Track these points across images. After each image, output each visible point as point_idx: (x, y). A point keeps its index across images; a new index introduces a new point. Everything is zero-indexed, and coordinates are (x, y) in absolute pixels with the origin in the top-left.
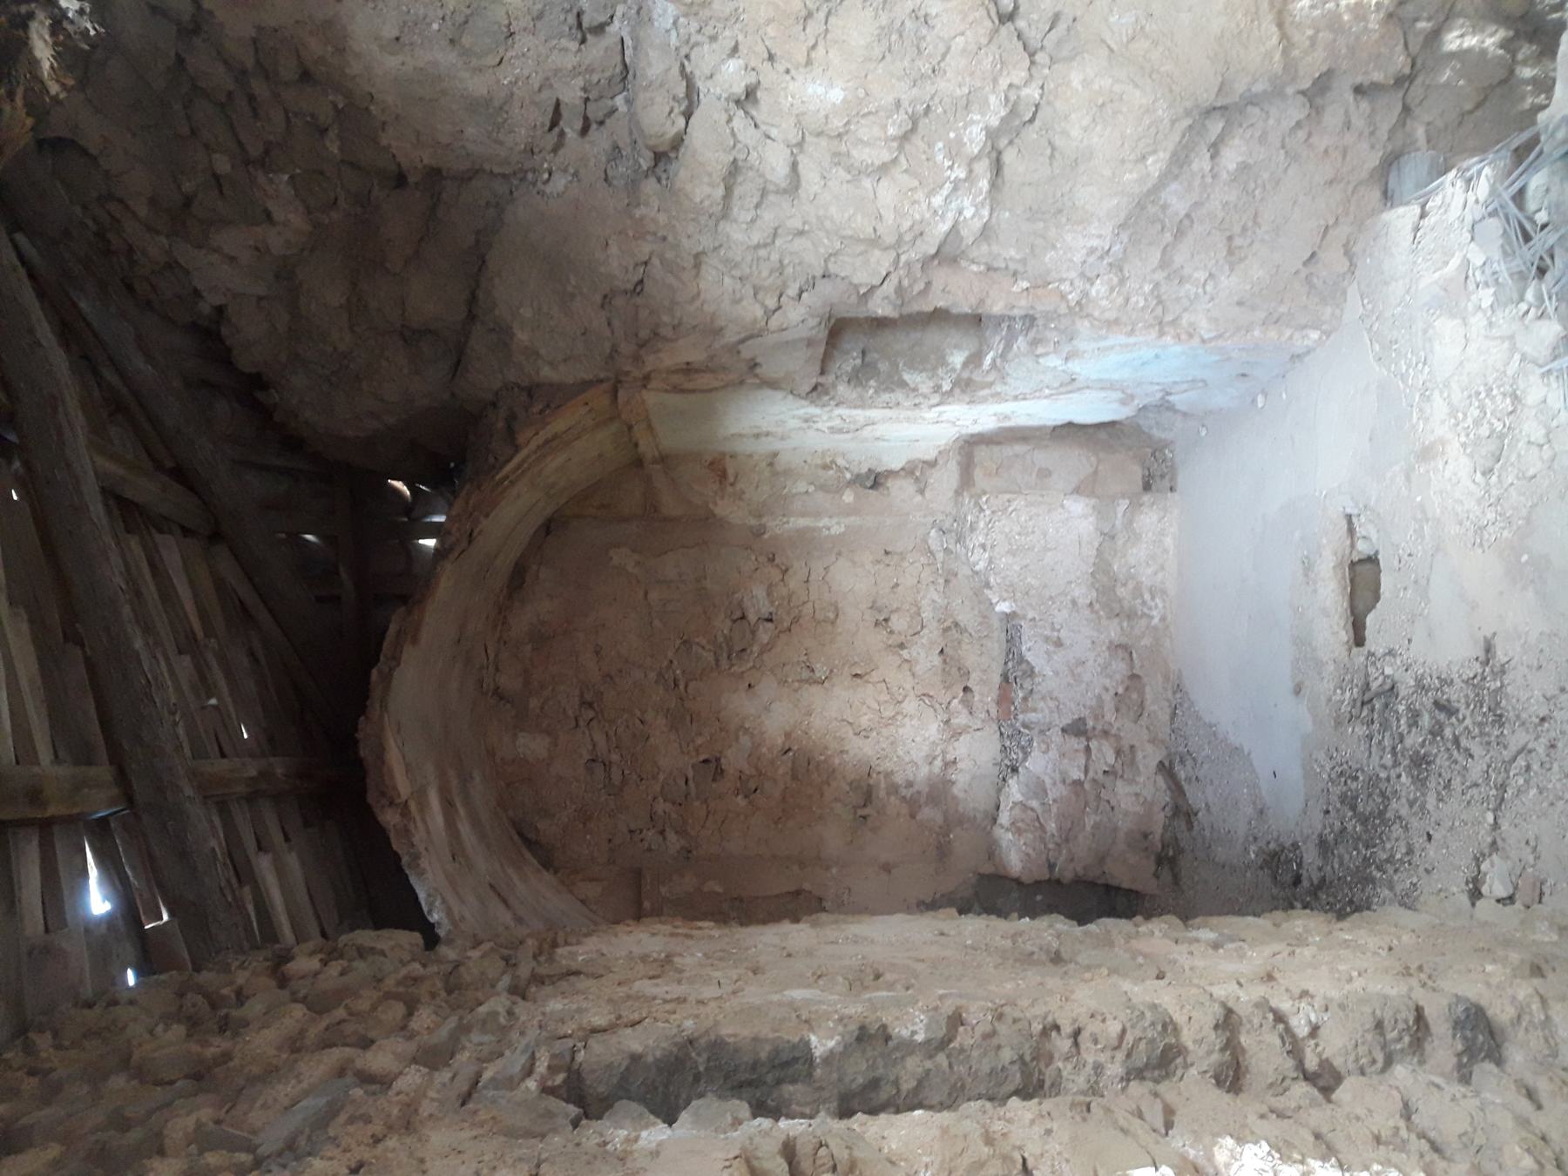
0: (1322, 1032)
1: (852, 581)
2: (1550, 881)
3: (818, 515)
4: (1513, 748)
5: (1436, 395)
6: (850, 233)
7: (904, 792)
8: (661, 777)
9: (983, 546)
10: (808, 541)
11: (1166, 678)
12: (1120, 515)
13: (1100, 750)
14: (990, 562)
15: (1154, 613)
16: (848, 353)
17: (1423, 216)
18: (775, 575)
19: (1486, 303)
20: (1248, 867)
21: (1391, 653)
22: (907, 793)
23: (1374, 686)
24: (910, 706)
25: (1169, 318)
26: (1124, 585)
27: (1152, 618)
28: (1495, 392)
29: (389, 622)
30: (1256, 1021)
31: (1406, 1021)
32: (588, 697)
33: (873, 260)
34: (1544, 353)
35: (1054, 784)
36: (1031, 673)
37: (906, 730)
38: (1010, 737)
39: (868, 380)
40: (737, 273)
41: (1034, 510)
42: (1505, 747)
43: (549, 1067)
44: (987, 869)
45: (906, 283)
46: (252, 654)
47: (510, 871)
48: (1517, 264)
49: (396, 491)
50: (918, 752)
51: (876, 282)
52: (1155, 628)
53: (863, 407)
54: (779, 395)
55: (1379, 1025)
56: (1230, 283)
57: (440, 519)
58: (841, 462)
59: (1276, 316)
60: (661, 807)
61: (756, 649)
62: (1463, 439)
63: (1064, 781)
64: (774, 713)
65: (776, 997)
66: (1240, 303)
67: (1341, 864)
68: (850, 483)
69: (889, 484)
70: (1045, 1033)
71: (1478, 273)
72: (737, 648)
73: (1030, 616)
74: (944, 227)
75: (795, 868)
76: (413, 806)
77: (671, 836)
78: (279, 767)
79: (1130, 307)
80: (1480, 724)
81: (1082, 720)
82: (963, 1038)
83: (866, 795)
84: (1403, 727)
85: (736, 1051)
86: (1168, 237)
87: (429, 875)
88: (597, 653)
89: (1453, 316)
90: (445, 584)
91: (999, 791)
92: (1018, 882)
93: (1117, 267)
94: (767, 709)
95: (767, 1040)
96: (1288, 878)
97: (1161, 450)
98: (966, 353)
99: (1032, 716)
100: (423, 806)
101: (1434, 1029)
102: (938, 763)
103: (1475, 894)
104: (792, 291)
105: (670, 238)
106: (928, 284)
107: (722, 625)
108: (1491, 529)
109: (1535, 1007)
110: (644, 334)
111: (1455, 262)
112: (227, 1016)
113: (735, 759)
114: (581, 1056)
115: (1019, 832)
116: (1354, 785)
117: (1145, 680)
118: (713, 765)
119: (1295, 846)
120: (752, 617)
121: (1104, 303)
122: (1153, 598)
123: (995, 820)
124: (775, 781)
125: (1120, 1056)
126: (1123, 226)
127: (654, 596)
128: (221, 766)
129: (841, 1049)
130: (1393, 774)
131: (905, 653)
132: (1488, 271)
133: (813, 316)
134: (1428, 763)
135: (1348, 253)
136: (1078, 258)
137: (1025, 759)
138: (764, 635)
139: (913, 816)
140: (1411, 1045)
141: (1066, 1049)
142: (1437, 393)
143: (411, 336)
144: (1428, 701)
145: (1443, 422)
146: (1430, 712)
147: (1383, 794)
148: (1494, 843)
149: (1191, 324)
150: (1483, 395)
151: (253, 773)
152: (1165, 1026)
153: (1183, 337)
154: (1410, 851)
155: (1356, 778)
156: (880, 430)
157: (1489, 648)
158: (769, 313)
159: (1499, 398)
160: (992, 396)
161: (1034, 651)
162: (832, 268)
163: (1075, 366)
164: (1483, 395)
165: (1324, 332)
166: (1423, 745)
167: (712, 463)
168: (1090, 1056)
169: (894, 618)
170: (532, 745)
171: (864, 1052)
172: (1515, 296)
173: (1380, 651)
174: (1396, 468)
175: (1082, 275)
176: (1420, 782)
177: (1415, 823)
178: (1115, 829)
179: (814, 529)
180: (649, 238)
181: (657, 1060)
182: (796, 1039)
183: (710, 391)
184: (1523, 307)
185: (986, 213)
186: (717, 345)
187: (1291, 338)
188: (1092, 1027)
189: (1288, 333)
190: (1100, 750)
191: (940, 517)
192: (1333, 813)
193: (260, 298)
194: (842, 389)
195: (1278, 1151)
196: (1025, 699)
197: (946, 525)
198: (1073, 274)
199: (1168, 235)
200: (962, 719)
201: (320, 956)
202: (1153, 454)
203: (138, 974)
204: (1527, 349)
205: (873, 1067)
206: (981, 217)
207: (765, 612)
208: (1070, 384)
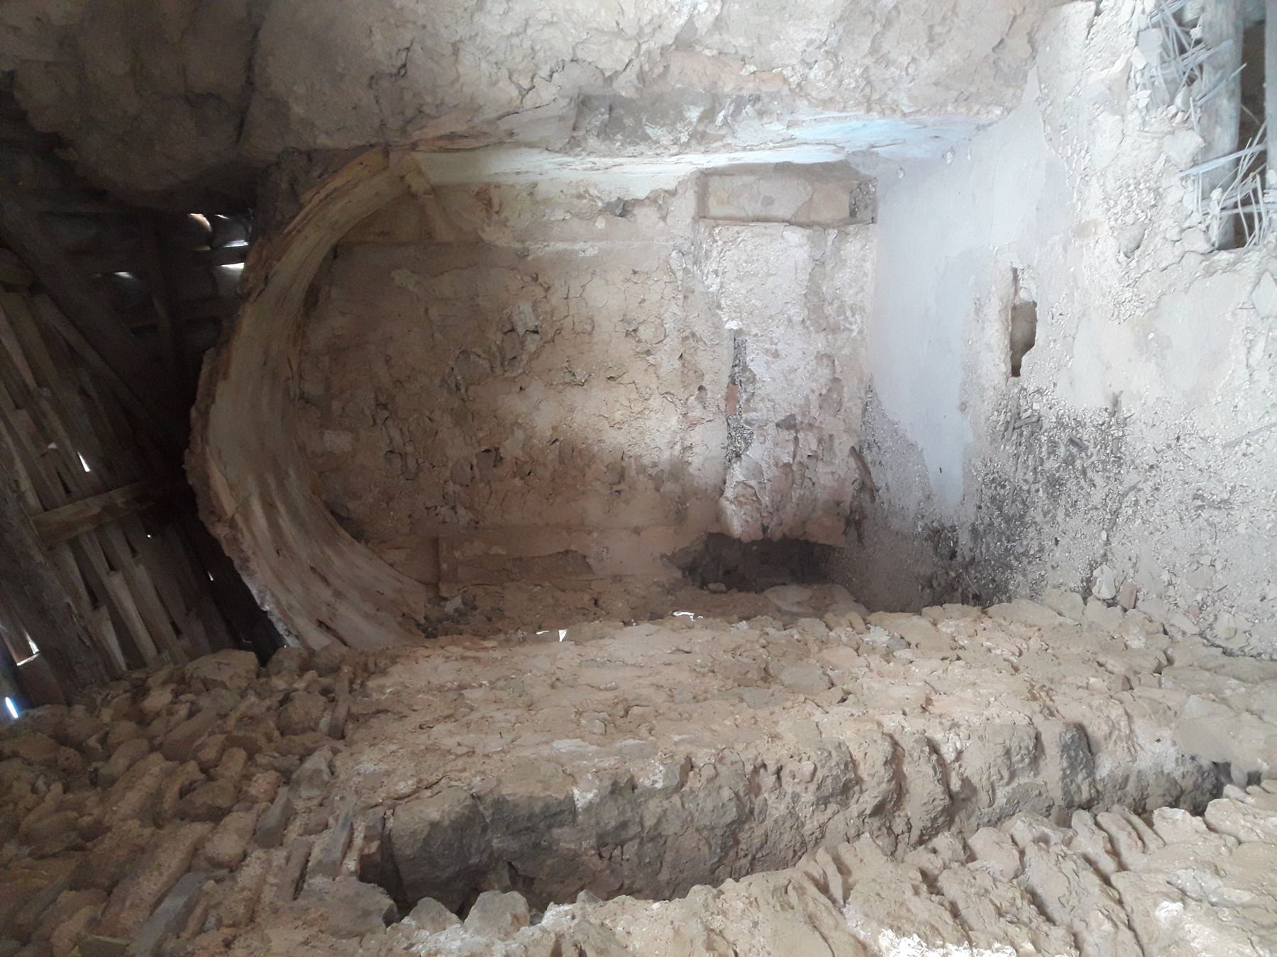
0: (965, 754)
1: (605, 298)
2: (1144, 591)
3: (574, 240)
4: (1127, 485)
5: (1094, 181)
6: (595, 25)
7: (650, 471)
8: (450, 465)
9: (716, 272)
10: (565, 262)
11: (861, 381)
12: (830, 243)
13: (805, 439)
14: (722, 287)
15: (854, 327)
16: (597, 109)
17: (1098, 13)
18: (539, 292)
19: (1142, 104)
20: (916, 537)
21: (1038, 391)
22: (653, 472)
23: (1024, 415)
24: (655, 402)
25: (875, 96)
26: (831, 304)
27: (852, 331)
28: (1141, 187)
29: (201, 362)
30: (916, 755)
31: (1027, 748)
32: (382, 399)
33: (617, 49)
34: (1186, 159)
35: (769, 467)
36: (753, 380)
37: (652, 422)
38: (736, 429)
39: (615, 134)
40: (493, 59)
41: (759, 241)
42: (1121, 483)
43: (365, 837)
44: (715, 530)
45: (646, 68)
46: (83, 392)
47: (329, 552)
48: (1172, 71)
49: (198, 223)
50: (662, 441)
51: (620, 68)
52: (855, 339)
53: (611, 156)
54: (536, 151)
55: (1008, 753)
56: (929, 66)
57: (241, 243)
58: (593, 192)
59: (966, 94)
60: (451, 488)
61: (525, 357)
62: (1112, 223)
63: (776, 465)
64: (541, 413)
65: (545, 751)
66: (936, 84)
67: (988, 550)
68: (601, 212)
69: (636, 211)
70: (756, 771)
71: (1138, 75)
72: (509, 356)
73: (753, 333)
74: (681, 21)
75: (564, 533)
76: (239, 519)
77: (462, 511)
78: (118, 498)
79: (842, 89)
80: (1103, 462)
81: (792, 416)
82: (693, 782)
83: (620, 475)
84: (1044, 454)
85: (516, 806)
86: (878, 27)
87: (258, 575)
88: (387, 362)
89: (1114, 112)
90: (251, 327)
91: (726, 469)
92: (739, 540)
93: (833, 54)
94: (536, 408)
95: (539, 798)
96: (945, 552)
97: (867, 185)
98: (702, 109)
99: (753, 415)
100: (247, 516)
101: (1047, 751)
102: (678, 447)
103: (1087, 593)
104: (544, 72)
105: (429, 27)
106: (666, 68)
107: (495, 337)
108: (1128, 305)
109: (1123, 723)
110: (409, 113)
111: (1120, 64)
112: (96, 770)
113: (511, 448)
114: (390, 824)
115: (741, 504)
116: (1002, 492)
117: (844, 382)
118: (493, 454)
119: (953, 529)
120: (521, 330)
121: (821, 84)
122: (853, 316)
123: (722, 492)
124: (545, 466)
125: (813, 787)
126: (841, 19)
127: (434, 313)
128: (66, 512)
129: (598, 800)
130: (1033, 488)
131: (650, 358)
132: (1147, 75)
133: (562, 97)
134: (1061, 485)
135: (1031, 41)
136: (799, 48)
137: (746, 449)
138: (531, 346)
139: (657, 490)
140: (1030, 764)
141: (771, 785)
142: (1094, 179)
143: (197, 101)
144: (1065, 436)
145: (1097, 206)
146: (1066, 446)
147: (1024, 503)
148: (1105, 555)
149: (895, 101)
150: (1132, 188)
151: (96, 510)
152: (846, 765)
153: (887, 112)
154: (1041, 550)
155: (1004, 487)
156: (626, 168)
157: (1116, 403)
158: (524, 93)
159: (1145, 191)
160: (724, 146)
161: (756, 362)
162: (580, 54)
163: (795, 132)
164: (1132, 188)
165: (1006, 109)
166: (1058, 470)
167: (478, 193)
168: (788, 787)
169: (641, 329)
170: (337, 441)
171: (616, 801)
172: (1167, 98)
173: (1031, 389)
174: (1056, 238)
175: (803, 61)
176: (1054, 499)
177: (1046, 529)
178: (815, 500)
179: (572, 252)
180: (410, 26)
181: (452, 822)
182: (562, 797)
183: (473, 149)
184: (1173, 109)
185: (718, 7)
186: (477, 121)
187: (978, 113)
188: (791, 766)
189: (976, 108)
190: (805, 439)
191: (679, 241)
192: (984, 509)
193: (48, 64)
194: (592, 142)
195: (926, 941)
196: (748, 401)
197: (685, 248)
198: (794, 61)
199: (878, 25)
200: (697, 413)
201: (173, 686)
202: (859, 186)
203: (20, 705)
204: (1172, 154)
205: (622, 813)
206: (713, 11)
207: (531, 326)
208: (790, 142)
